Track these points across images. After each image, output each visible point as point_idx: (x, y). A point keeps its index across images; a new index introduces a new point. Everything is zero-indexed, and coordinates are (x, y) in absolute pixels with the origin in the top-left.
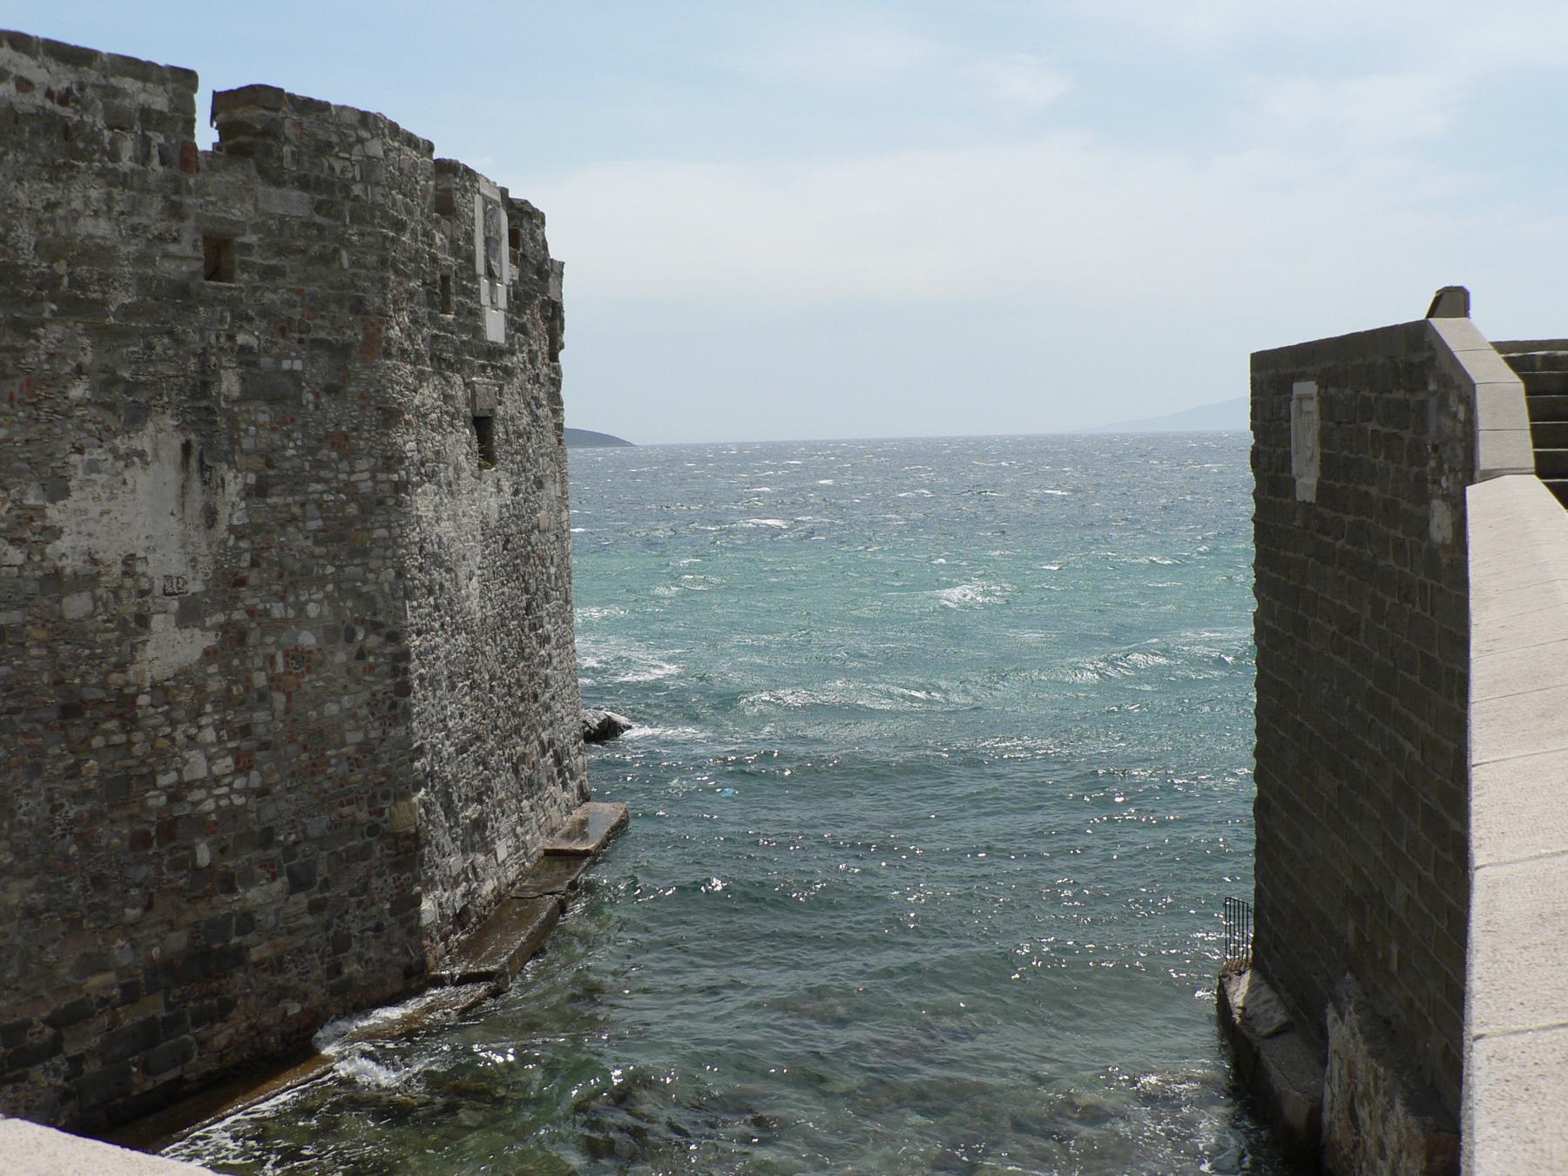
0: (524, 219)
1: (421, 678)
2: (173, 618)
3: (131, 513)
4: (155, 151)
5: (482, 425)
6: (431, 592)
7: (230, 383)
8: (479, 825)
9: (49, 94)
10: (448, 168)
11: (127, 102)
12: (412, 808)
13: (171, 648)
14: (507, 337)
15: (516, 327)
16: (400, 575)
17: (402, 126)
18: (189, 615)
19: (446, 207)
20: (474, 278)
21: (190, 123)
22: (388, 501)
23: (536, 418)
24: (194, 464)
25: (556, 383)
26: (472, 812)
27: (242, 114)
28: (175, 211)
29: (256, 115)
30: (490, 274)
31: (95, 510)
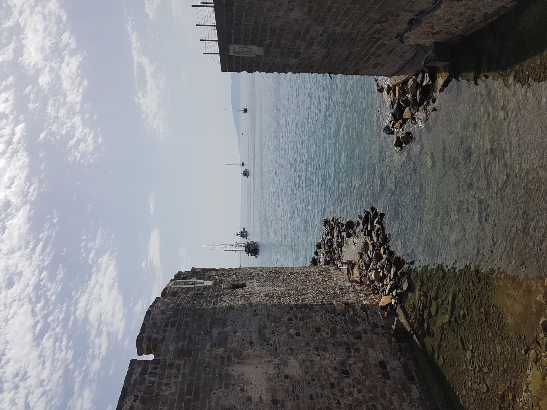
0: (179, 276)
1: (302, 301)
2: (285, 368)
3: (255, 375)
4: (153, 371)
5: (235, 287)
6: (279, 299)
7: (220, 351)
8: (341, 289)
9: (135, 401)
10: (164, 293)
11: (139, 379)
12: (338, 305)
13: (294, 368)
14: (211, 280)
15: (209, 278)
16: (275, 306)
17: (151, 304)
18: (285, 363)
19: (175, 294)
20: (195, 288)
21: (146, 362)
22: (255, 310)
23: (234, 274)
24: (242, 361)
25: (223, 270)
26: (338, 291)
27: (144, 347)
28: (171, 366)
29: (144, 342)
30: (194, 284)
31: (255, 389)
